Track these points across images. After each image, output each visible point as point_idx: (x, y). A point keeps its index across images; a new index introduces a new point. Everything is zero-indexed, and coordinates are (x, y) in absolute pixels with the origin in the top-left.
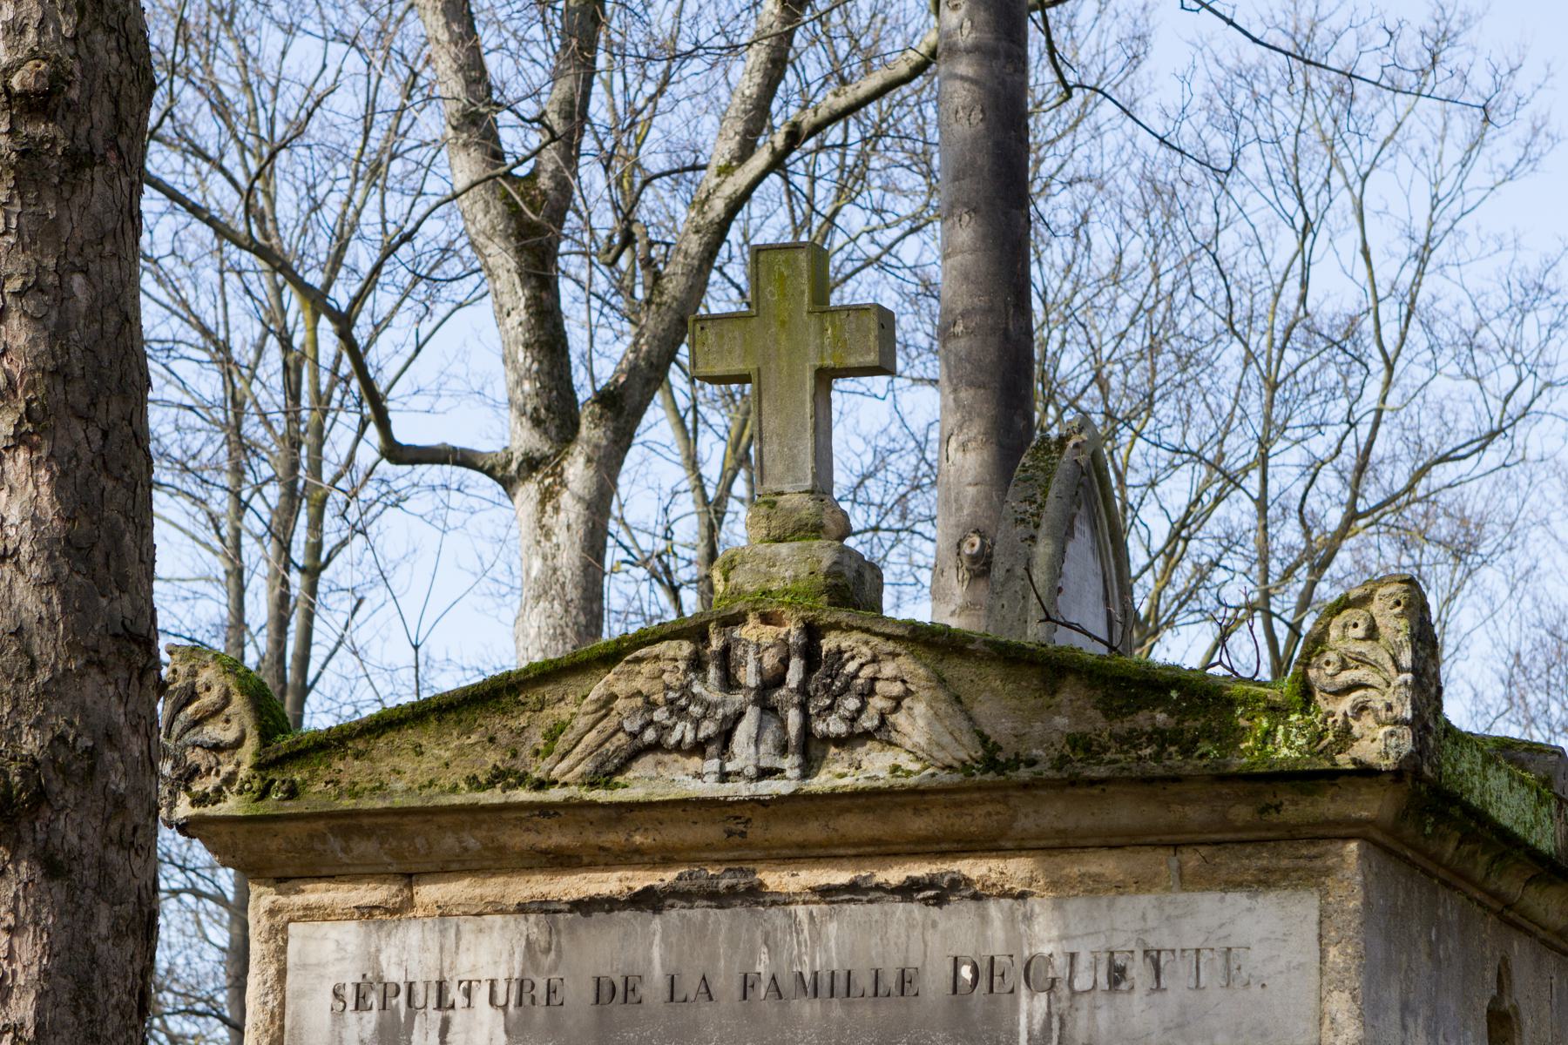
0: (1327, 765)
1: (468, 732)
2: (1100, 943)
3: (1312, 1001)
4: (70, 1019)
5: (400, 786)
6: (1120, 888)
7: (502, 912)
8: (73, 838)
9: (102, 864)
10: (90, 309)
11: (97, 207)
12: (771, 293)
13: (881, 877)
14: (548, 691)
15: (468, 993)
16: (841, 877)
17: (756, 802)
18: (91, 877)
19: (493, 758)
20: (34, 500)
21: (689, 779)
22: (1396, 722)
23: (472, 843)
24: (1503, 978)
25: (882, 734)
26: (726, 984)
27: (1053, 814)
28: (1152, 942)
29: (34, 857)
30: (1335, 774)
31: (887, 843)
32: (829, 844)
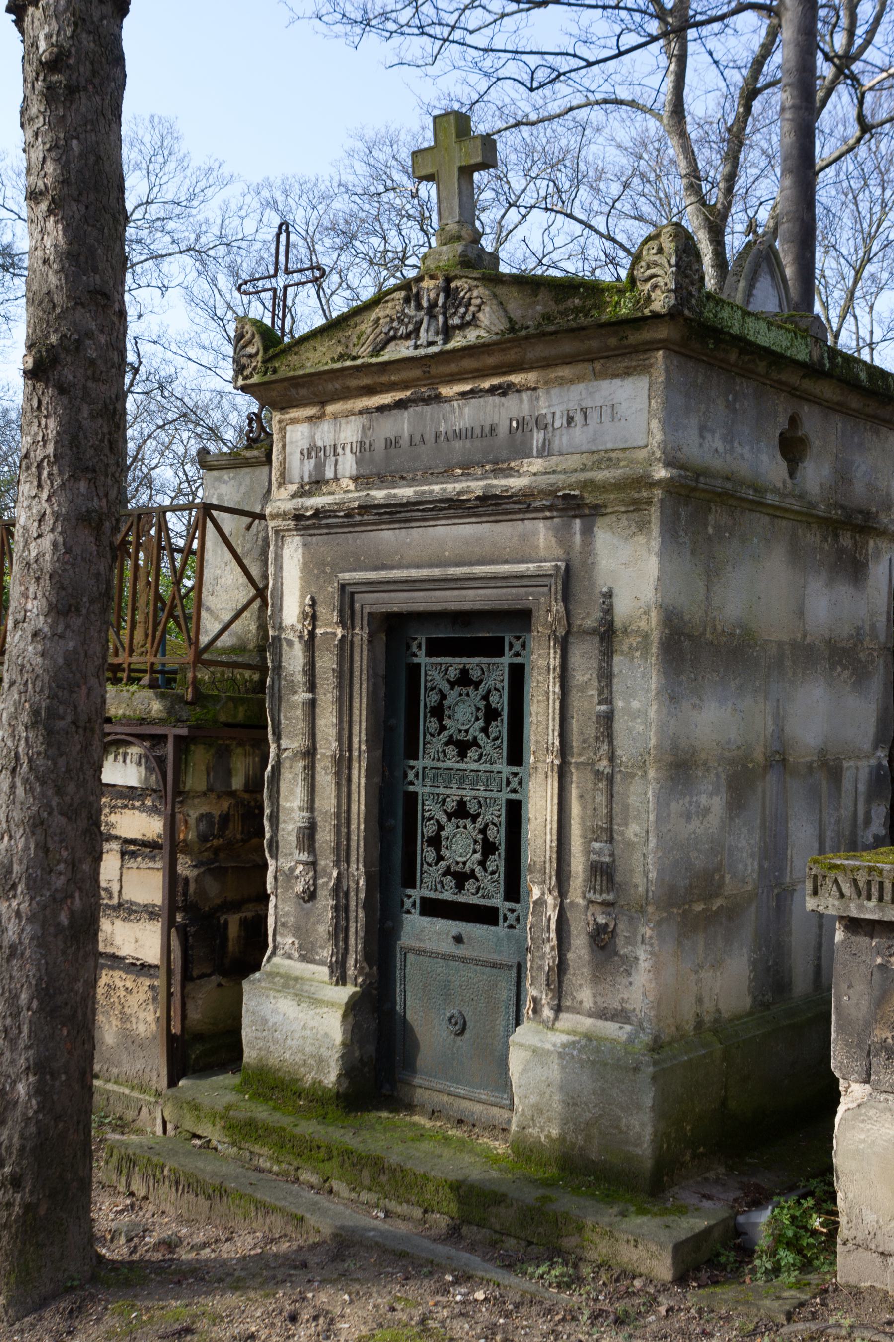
0: (640, 314)
1: (331, 340)
2: (563, 407)
3: (645, 425)
4: (68, 452)
5: (309, 365)
6: (571, 382)
7: (354, 414)
9: (85, 387)
10: (81, 154)
11: (83, 110)
12: (441, 136)
13: (482, 386)
14: (357, 319)
15: (343, 449)
16: (467, 387)
17: (426, 356)
18: (80, 393)
19: (340, 349)
20: (56, 237)
21: (403, 350)
22: (669, 291)
23: (337, 386)
24: (794, 421)
25: (473, 322)
26: (430, 437)
27: (538, 351)
28: (584, 405)
29: (54, 386)
30: (644, 319)
31: (482, 370)
32: (460, 373)
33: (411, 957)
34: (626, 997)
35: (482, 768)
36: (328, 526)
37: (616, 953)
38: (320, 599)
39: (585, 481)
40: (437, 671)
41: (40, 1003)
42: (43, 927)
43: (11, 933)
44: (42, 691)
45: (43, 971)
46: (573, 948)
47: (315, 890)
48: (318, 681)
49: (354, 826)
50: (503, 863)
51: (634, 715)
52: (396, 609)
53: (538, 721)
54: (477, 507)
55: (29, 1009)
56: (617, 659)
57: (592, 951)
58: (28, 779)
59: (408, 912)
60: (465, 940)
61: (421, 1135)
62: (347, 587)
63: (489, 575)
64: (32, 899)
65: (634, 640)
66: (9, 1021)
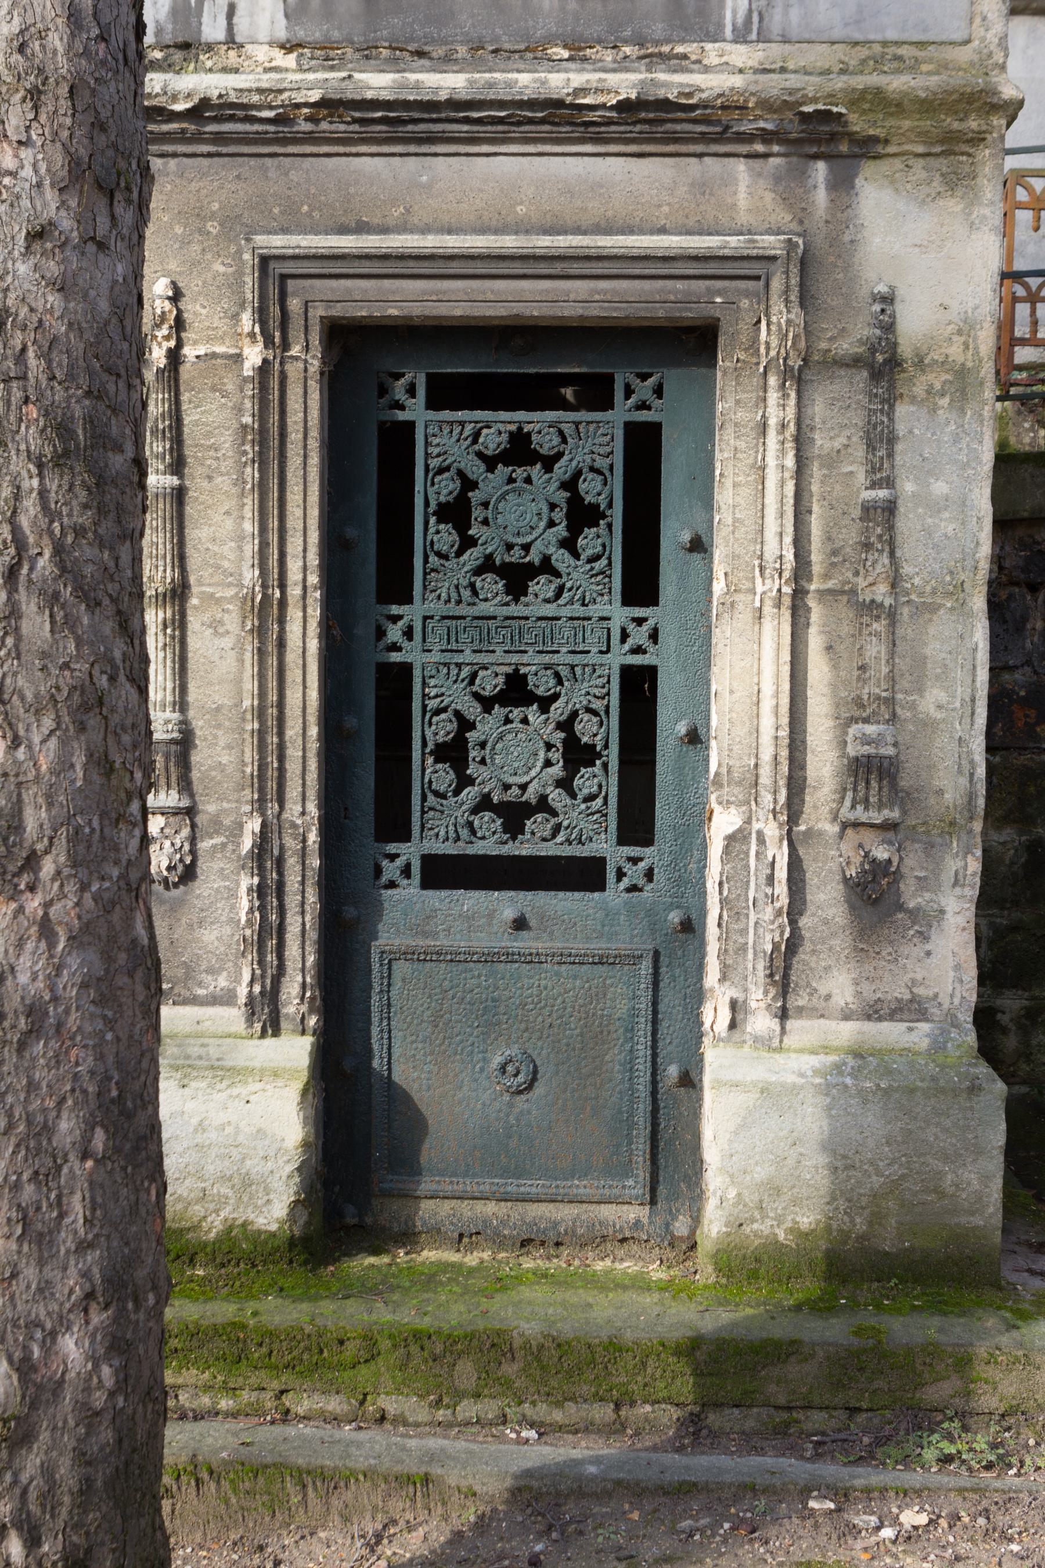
8: (805, 1220)
33: (401, 968)
34: (919, 977)
35: (566, 612)
36: (219, 138)
37: (900, 907)
38: (191, 286)
39: (865, 91)
40: (447, 441)
41: (112, 1135)
42: (107, 957)
43: (23, 978)
44: (71, 376)
45: (111, 1059)
46: (811, 909)
47: (194, 862)
48: (187, 452)
49: (292, 731)
50: (614, 779)
51: (936, 507)
52: (393, 312)
53: (735, 520)
54: (610, 122)
55: (85, 1156)
56: (902, 410)
57: (852, 908)
58: (56, 596)
59: (392, 885)
60: (533, 923)
61: (430, 1279)
62: (272, 265)
63: (635, 252)
64: (84, 887)
65: (937, 379)
66: (29, 1192)
